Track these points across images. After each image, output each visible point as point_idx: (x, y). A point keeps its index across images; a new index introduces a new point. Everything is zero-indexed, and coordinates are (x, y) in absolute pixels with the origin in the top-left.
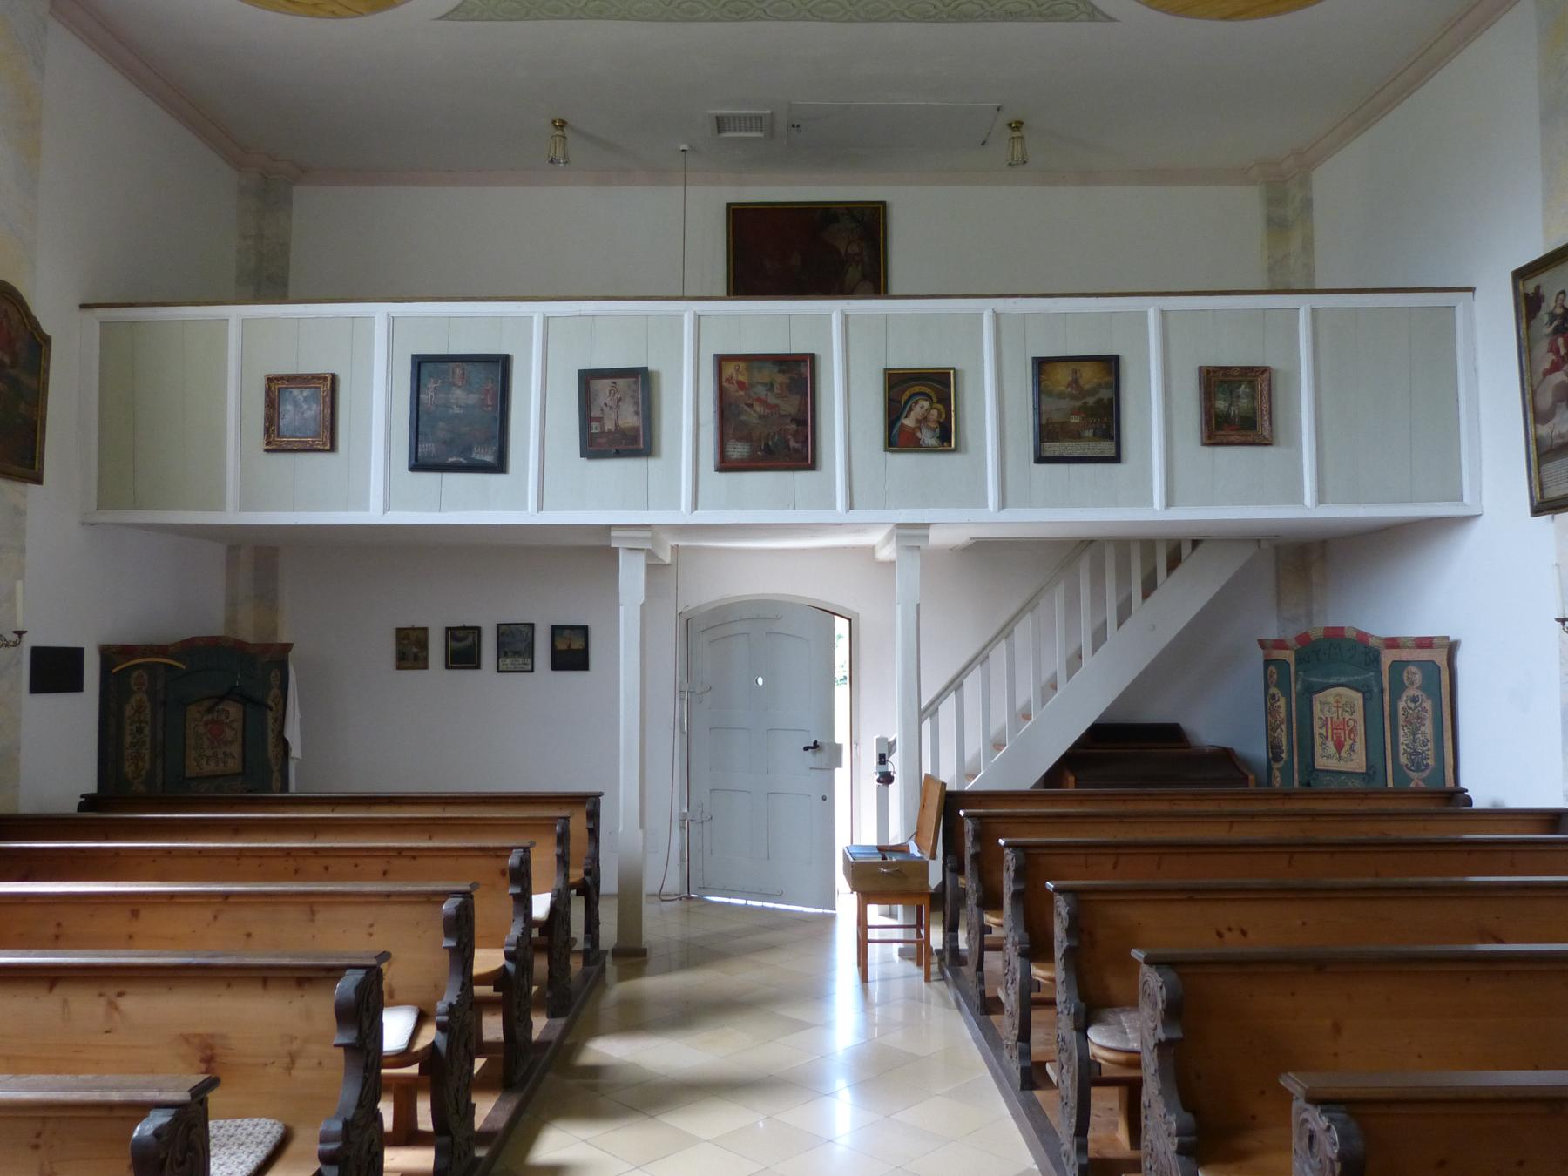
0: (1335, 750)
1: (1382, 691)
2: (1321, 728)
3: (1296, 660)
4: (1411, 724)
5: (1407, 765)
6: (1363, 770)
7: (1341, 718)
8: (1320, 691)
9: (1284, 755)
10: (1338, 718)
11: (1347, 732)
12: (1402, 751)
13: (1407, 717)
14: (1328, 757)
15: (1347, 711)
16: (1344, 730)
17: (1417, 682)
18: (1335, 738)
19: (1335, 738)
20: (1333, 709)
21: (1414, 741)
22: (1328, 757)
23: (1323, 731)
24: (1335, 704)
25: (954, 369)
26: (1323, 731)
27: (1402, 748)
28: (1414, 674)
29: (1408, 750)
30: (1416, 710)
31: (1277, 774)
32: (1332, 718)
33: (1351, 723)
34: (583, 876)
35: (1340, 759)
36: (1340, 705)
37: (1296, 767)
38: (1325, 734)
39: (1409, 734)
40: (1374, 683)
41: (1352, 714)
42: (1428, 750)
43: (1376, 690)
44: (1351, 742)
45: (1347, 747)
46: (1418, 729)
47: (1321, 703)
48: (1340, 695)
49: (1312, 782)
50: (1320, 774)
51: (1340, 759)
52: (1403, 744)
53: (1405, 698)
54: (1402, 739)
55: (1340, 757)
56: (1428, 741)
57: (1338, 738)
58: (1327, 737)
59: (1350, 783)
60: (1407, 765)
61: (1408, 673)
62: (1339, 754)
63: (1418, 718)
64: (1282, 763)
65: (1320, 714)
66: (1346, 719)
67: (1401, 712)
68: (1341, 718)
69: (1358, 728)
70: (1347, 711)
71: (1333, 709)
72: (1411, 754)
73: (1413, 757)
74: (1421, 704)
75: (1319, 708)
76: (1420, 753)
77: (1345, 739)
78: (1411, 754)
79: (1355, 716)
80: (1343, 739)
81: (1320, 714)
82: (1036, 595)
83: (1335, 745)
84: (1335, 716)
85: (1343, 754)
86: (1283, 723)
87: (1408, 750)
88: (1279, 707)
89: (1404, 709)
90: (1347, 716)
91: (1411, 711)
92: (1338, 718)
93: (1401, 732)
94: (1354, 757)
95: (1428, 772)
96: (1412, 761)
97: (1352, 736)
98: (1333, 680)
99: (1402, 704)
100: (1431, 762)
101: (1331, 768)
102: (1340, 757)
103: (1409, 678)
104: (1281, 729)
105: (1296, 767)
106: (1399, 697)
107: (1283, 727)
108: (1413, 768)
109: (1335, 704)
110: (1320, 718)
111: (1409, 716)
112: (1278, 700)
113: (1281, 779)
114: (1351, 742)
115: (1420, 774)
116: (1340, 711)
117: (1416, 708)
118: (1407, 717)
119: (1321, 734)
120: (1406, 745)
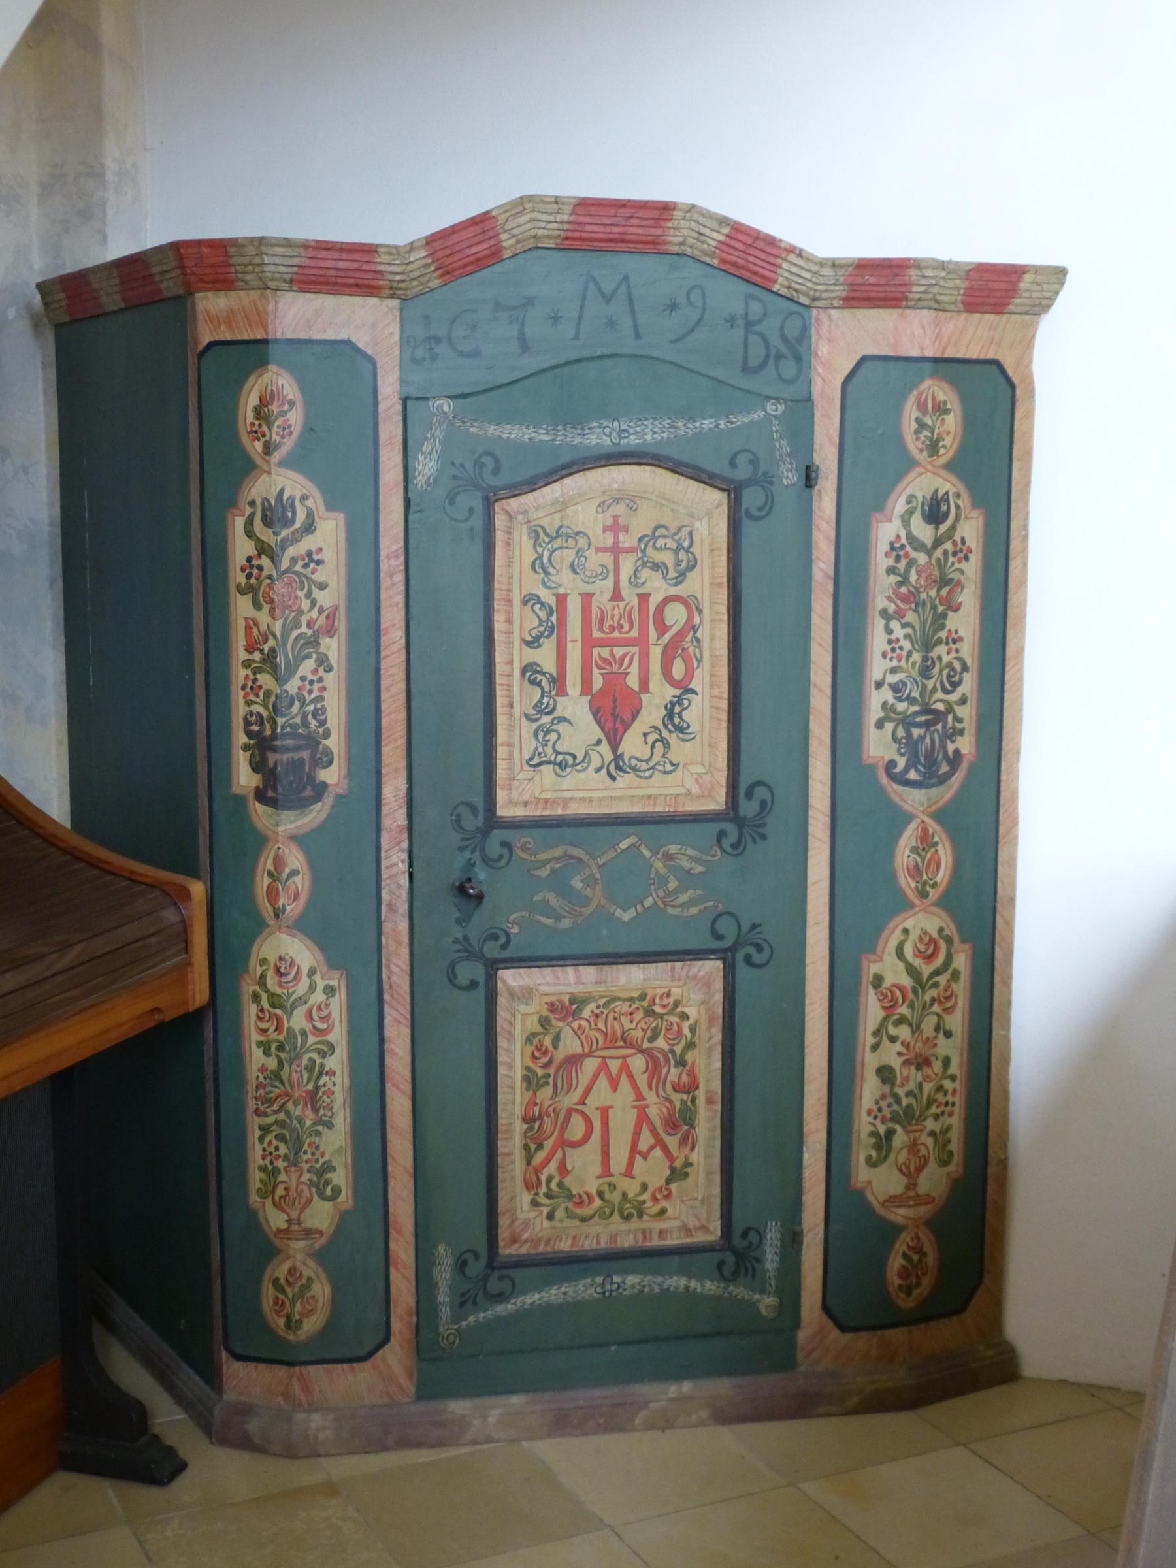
0: (598, 733)
1: (809, 478)
2: (533, 643)
3: (406, 340)
4: (919, 606)
5: (892, 764)
6: (717, 802)
7: (630, 596)
8: (532, 484)
9: (331, 776)
10: (616, 596)
11: (656, 653)
12: (874, 711)
13: (904, 581)
14: (562, 765)
15: (656, 567)
16: (642, 642)
17: (947, 441)
18: (598, 682)
19: (598, 682)
20: (595, 560)
21: (925, 672)
22: (562, 765)
23: (546, 658)
24: (609, 539)
25: (469, 1251)
26: (546, 658)
27: (876, 701)
28: (940, 409)
29: (901, 706)
30: (938, 553)
31: (295, 859)
32: (587, 598)
33: (676, 615)
34: (270, 1068)
35: (618, 766)
36: (626, 541)
37: (394, 815)
38: (550, 666)
39: (907, 645)
40: (784, 446)
41: (680, 579)
42: (963, 701)
43: (790, 477)
44: (671, 692)
45: (652, 713)
46: (939, 620)
47: (536, 534)
48: (630, 500)
49: (482, 874)
50: (519, 839)
51: (618, 766)
52: (879, 685)
53: (900, 507)
54: (877, 668)
55: (617, 758)
56: (965, 668)
57: (615, 680)
58: (559, 682)
59: (658, 865)
60: (892, 764)
61: (921, 406)
62: (614, 745)
63: (944, 581)
64: (316, 814)
65: (533, 584)
66: (654, 601)
67: (881, 560)
68: (630, 596)
69: (704, 633)
70: (656, 567)
71: (595, 560)
72: (907, 722)
73: (916, 732)
74: (953, 528)
75: (529, 555)
76: (938, 716)
77: (644, 685)
78: (907, 722)
79: (693, 585)
80: (633, 681)
81: (533, 584)
82: (1006, 1474)
83: (596, 712)
84: (602, 599)
85: (633, 744)
86: (330, 631)
87: (901, 706)
88: (311, 559)
89: (894, 548)
90: (658, 588)
91: (922, 558)
92: (616, 596)
93: (877, 641)
94: (680, 750)
95: (957, 779)
96: (910, 746)
97: (678, 669)
98: (598, 438)
99: (886, 531)
100: (965, 745)
101: (574, 810)
102: (617, 758)
103: (922, 425)
104: (322, 660)
105: (394, 815)
106: (879, 503)
107: (333, 647)
108: (913, 775)
109: (609, 539)
110: (530, 600)
111: (913, 577)
112: (309, 528)
113: (316, 881)
114: (671, 692)
115: (934, 791)
116: (626, 570)
117: (937, 543)
118: (904, 581)
119: (530, 671)
120: (896, 688)
